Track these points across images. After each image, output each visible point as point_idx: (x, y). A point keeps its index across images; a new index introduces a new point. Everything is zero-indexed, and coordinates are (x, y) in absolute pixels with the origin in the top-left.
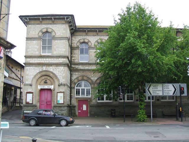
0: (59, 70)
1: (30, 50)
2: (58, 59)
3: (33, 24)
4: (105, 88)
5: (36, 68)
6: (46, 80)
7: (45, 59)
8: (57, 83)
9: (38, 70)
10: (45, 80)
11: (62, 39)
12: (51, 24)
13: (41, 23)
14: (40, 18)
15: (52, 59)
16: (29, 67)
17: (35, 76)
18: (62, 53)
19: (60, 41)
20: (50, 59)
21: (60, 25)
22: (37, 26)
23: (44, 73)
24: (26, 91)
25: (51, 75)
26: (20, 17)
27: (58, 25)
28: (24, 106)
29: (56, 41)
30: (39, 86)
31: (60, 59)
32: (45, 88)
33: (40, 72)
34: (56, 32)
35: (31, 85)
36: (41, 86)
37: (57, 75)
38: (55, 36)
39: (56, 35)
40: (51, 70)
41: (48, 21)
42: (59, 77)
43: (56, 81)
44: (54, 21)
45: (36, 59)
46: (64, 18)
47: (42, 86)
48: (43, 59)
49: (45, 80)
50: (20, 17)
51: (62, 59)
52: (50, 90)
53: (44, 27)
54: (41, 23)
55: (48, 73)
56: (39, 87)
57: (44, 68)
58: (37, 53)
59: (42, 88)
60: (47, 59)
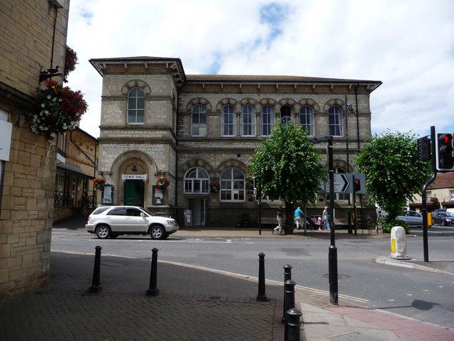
7: (133, 132)
9: (122, 149)
12: (143, 74)
15: (145, 132)
20: (141, 132)
23: (132, 155)
30: (123, 175)
33: (125, 153)
48: (129, 132)
51: (161, 132)
57: (132, 147)
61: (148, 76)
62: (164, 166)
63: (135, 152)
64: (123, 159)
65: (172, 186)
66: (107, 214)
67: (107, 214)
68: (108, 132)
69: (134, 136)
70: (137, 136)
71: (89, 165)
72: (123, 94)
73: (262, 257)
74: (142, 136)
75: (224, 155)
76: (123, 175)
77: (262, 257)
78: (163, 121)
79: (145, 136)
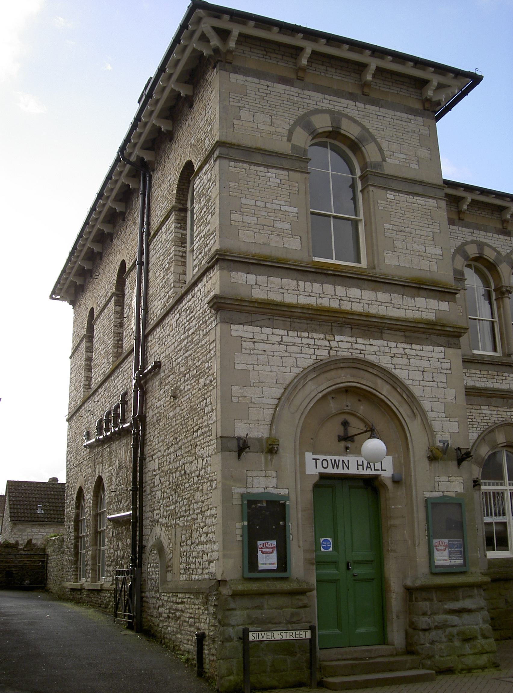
0: (425, 364)
1: (246, 219)
2: (413, 297)
3: (259, 75)
4: (196, 558)
5: (292, 337)
6: (345, 424)
7: (340, 290)
8: (419, 444)
9: (306, 348)
10: (342, 418)
11: (418, 189)
12: (352, 96)
13: (297, 78)
14: (374, 63)
15: (382, 296)
16: (248, 328)
17: (291, 389)
18: (425, 265)
19: (410, 198)
20: (368, 295)
21: (398, 114)
22: (280, 88)
23: (345, 378)
24: (243, 490)
25: (385, 391)
26: (475, 79)
27: (391, 112)
28: (235, 595)
29: (391, 195)
30: (309, 456)
31: (421, 301)
32: (346, 471)
33: (322, 368)
34: (385, 145)
35: (271, 448)
36: (322, 457)
37: (417, 391)
38: (378, 165)
39: (384, 160)
40: (384, 361)
41: (336, 78)
42: (426, 405)
43: (414, 427)
44: (303, 69)
45: (289, 283)
46: (362, 67)
47: (328, 458)
48: (328, 288)
49: (342, 418)
50: (475, 79)
51: (434, 304)
52: (371, 484)
53: (323, 105)
54: (301, 79)
55: (366, 381)
56: (314, 466)
57: (345, 345)
58: (293, 246)
59: (330, 470)
60: (355, 292)
61: (371, 108)
62: (453, 427)
63: (357, 364)
64: (314, 389)
65: (208, 409)
66: (214, 28)
67: (214, 28)
68: (251, 278)
69: (346, 306)
70: (357, 308)
71: (89, 369)
72: (294, 147)
73: (316, 468)
74: (373, 310)
75: (485, 410)
76: (309, 456)
77: (316, 468)
78: (435, 268)
79: (383, 311)
